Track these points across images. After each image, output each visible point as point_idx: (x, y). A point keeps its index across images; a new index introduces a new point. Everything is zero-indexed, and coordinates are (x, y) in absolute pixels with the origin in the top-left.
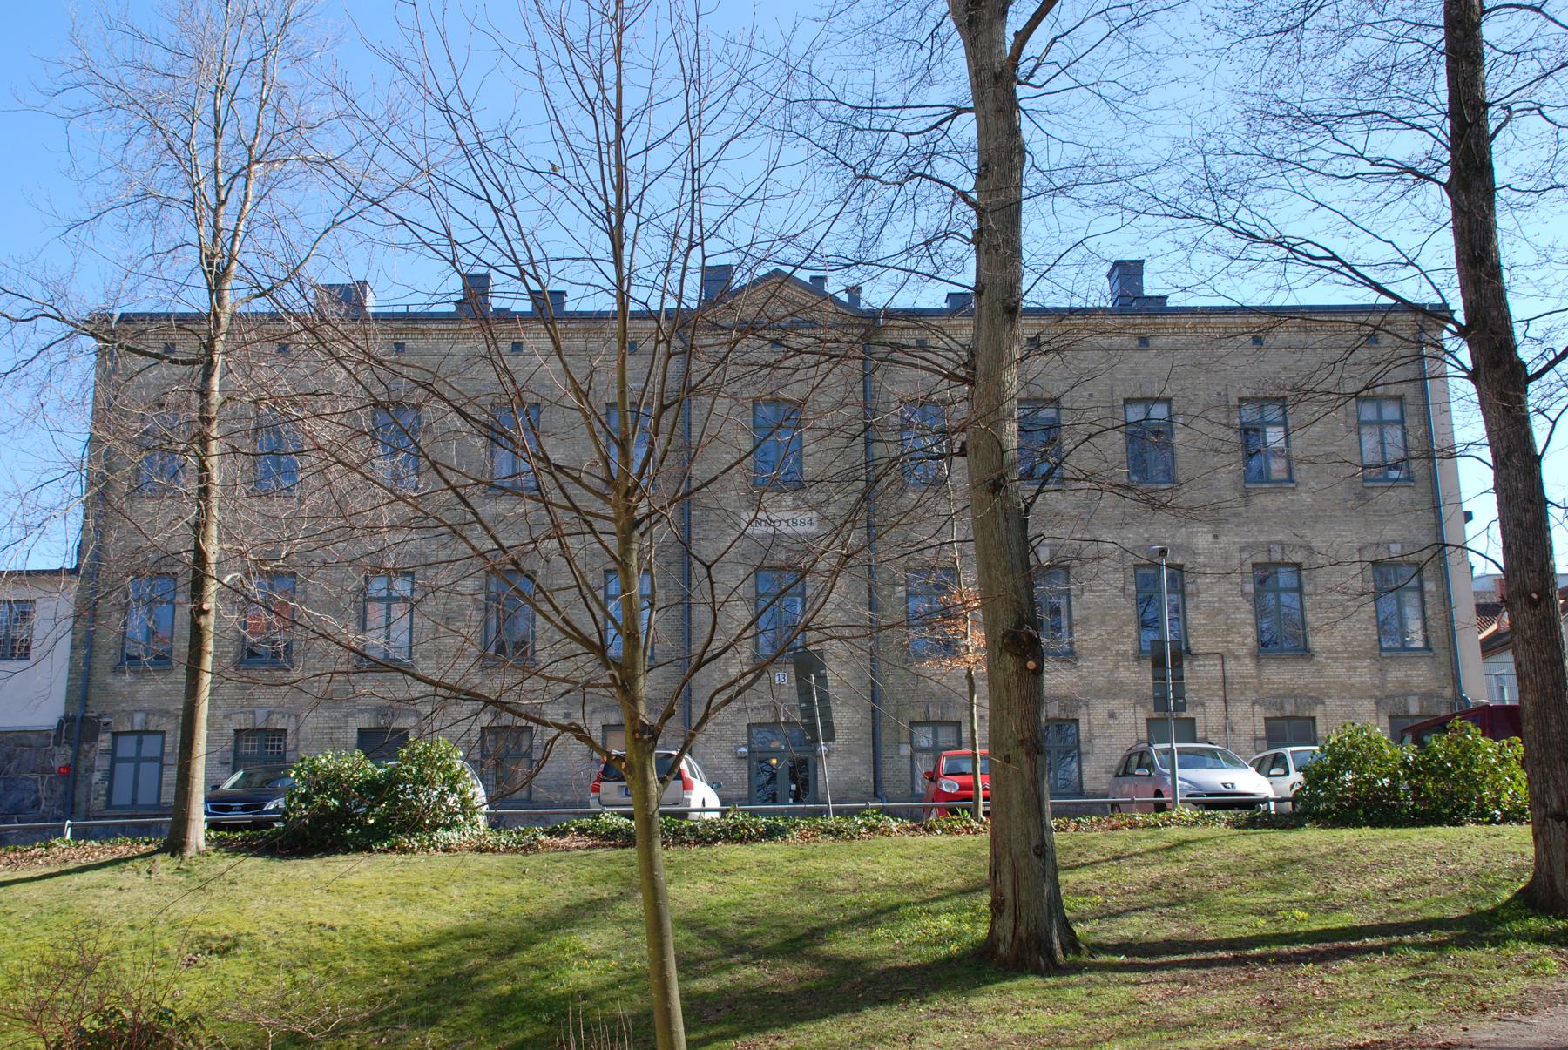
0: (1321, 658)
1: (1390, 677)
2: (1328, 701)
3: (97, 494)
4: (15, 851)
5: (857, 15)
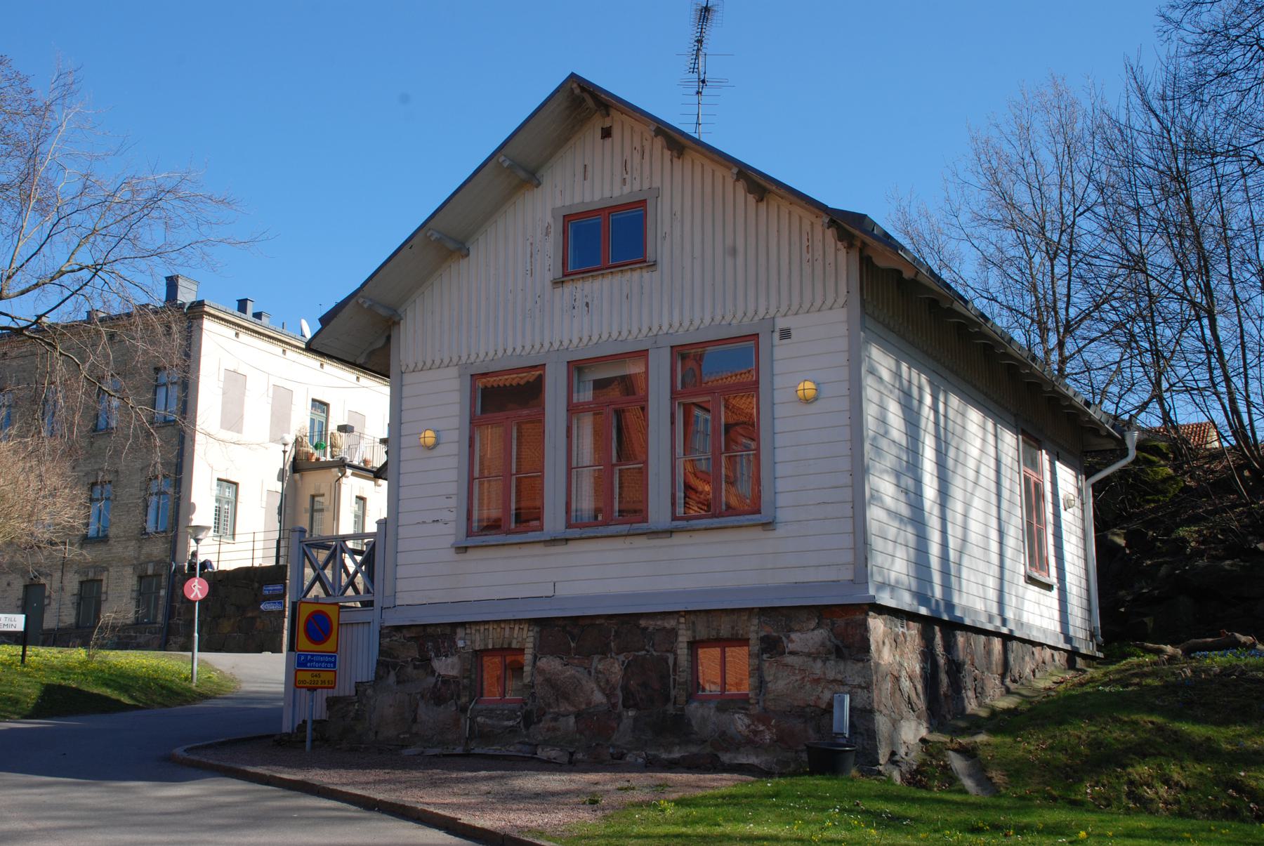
0: (111, 542)
1: (144, 551)
2: (111, 569)
3: (552, 708)
4: (870, 789)
5: (1262, 341)
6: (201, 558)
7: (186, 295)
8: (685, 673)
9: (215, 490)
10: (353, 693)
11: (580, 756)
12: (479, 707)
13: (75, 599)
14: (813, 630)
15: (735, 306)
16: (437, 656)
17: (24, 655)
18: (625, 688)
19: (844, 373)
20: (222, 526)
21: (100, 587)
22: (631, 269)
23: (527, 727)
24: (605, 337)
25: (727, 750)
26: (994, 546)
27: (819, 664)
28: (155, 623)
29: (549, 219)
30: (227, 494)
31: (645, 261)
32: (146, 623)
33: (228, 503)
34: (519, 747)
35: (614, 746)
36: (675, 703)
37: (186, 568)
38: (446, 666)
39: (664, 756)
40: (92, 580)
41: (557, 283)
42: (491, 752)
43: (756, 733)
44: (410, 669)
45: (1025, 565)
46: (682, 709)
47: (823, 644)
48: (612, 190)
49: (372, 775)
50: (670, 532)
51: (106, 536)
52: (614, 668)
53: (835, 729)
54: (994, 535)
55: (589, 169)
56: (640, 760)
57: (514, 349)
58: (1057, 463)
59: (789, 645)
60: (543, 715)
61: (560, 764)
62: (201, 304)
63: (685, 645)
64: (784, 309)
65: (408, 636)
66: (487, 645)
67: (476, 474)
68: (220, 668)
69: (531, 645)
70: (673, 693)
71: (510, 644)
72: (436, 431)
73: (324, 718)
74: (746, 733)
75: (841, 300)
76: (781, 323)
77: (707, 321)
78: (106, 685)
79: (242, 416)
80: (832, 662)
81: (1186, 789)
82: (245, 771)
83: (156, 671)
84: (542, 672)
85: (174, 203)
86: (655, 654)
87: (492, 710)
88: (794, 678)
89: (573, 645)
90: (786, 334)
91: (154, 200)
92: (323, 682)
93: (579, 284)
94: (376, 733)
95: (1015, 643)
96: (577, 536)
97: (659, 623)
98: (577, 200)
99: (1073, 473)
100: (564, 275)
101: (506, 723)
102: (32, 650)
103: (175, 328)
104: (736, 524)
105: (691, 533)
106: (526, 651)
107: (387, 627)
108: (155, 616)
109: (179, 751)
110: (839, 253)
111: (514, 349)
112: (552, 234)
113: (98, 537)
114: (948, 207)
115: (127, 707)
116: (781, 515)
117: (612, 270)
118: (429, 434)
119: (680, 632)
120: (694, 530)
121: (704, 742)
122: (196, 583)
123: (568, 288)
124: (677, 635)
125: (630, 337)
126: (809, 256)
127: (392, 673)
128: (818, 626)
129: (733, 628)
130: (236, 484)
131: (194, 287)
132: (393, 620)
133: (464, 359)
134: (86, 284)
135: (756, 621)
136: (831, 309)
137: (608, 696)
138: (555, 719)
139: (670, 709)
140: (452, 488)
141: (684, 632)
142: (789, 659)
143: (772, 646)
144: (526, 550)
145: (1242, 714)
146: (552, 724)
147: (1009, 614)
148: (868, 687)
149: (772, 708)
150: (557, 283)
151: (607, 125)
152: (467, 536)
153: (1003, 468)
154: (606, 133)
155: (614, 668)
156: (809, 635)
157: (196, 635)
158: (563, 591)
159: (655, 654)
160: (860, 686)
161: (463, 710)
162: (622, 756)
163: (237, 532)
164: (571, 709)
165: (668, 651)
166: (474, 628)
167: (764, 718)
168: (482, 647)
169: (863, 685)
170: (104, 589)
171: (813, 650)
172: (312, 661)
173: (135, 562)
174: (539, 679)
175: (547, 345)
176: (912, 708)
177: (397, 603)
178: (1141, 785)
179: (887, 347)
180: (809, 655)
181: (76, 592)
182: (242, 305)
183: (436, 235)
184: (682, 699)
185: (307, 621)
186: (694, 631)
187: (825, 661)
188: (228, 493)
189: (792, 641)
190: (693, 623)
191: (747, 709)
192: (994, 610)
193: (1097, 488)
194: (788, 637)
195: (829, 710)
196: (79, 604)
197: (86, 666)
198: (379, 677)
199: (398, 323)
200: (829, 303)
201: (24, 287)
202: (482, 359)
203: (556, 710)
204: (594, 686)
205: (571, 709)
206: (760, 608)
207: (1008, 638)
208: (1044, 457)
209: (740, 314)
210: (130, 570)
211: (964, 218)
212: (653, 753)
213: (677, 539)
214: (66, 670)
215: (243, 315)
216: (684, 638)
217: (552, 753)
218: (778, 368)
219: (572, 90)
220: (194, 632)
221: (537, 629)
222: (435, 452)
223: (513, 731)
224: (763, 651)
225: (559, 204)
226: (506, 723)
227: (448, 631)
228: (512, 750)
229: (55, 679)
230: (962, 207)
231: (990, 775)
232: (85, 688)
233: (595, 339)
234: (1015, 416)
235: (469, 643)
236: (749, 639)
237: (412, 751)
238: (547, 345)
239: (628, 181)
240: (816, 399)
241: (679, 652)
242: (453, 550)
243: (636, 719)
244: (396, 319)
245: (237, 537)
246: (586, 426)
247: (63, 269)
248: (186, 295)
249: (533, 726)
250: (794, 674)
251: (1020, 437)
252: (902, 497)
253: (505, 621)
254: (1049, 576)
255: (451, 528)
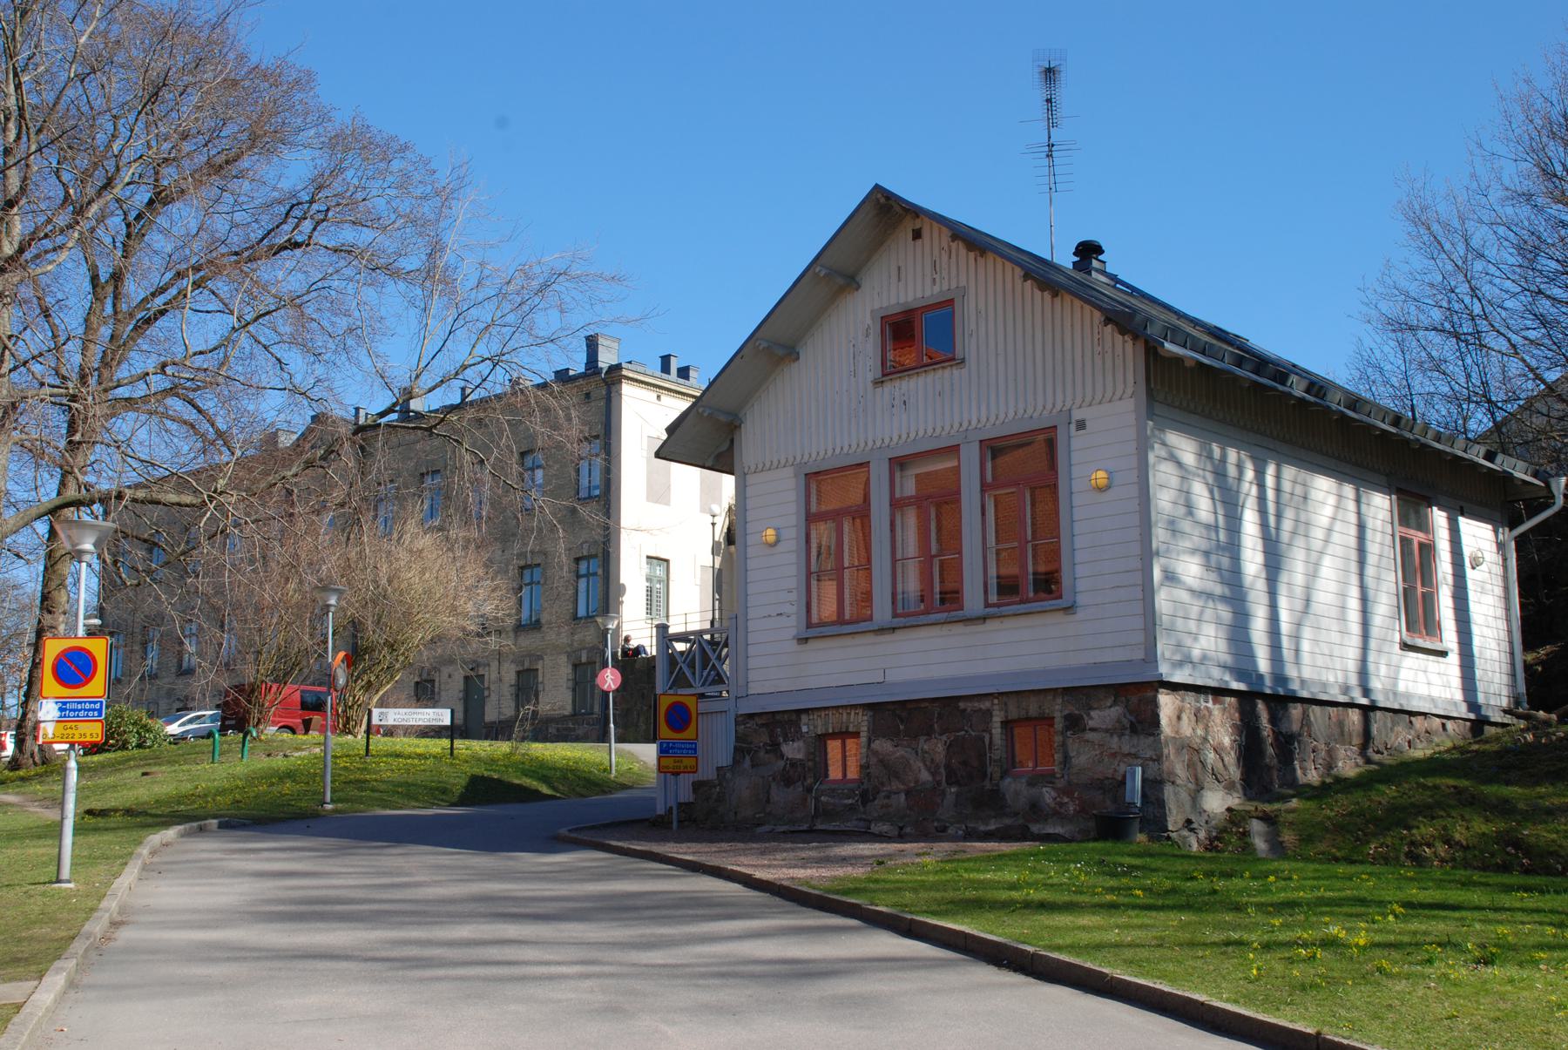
0: (544, 629)
6: (633, 644)
7: (606, 359)
8: (999, 752)
9: (645, 569)
10: (715, 777)
11: (908, 830)
12: (823, 787)
13: (513, 690)
14: (1111, 707)
15: (1035, 400)
16: (785, 741)
17: (452, 748)
18: (947, 766)
19: (1134, 462)
20: (654, 608)
21: (536, 677)
22: (934, 369)
23: (864, 803)
24: (921, 433)
25: (1037, 821)
26: (1354, 616)
27: (1116, 739)
28: (592, 714)
29: (869, 321)
30: (658, 572)
31: (954, 359)
32: (584, 714)
33: (659, 582)
34: (855, 823)
35: (938, 820)
36: (991, 779)
37: (619, 654)
38: (793, 750)
39: (982, 828)
40: (528, 670)
41: (878, 383)
42: (831, 828)
43: (1061, 804)
44: (762, 754)
45: (1400, 631)
46: (997, 785)
47: (1119, 721)
48: (924, 291)
49: (714, 847)
50: (984, 619)
51: (538, 621)
52: (937, 747)
53: (1128, 799)
54: (1354, 604)
55: (903, 268)
56: (960, 832)
57: (842, 449)
58: (1461, 519)
59: (1090, 722)
60: (878, 793)
61: (890, 837)
62: (618, 367)
63: (999, 725)
64: (1079, 401)
65: (759, 723)
66: (827, 729)
67: (814, 568)
68: (644, 759)
69: (866, 729)
70: (989, 770)
71: (847, 727)
72: (777, 529)
73: (691, 800)
74: (1053, 805)
75: (1129, 391)
76: (1077, 415)
77: (1011, 414)
78: (526, 773)
79: (669, 487)
80: (1127, 737)
81: (1466, 848)
82: (609, 845)
83: (577, 763)
84: (876, 753)
85: (567, 284)
86: (973, 734)
87: (834, 790)
88: (1094, 753)
89: (902, 727)
90: (1081, 425)
91: (545, 286)
92: (686, 767)
93: (897, 383)
94: (736, 813)
95: (1379, 713)
96: (901, 625)
97: (976, 704)
98: (893, 301)
99: (1490, 527)
100: (884, 375)
101: (846, 801)
102: (458, 743)
103: (574, 414)
104: (1039, 609)
105: (1002, 619)
106: (862, 734)
107: (742, 715)
108: (592, 707)
109: (563, 831)
110: (1126, 345)
111: (842, 449)
112: (871, 336)
113: (531, 624)
114: (1474, 185)
115: (559, 798)
116: (1081, 599)
117: (926, 369)
118: (770, 532)
119: (994, 713)
120: (1004, 616)
121: (1016, 814)
122: (608, 674)
123: (888, 387)
124: (991, 716)
125: (943, 433)
126: (1100, 349)
127: (748, 758)
128: (1115, 703)
129: (1040, 707)
130: (667, 561)
131: (615, 345)
132: (746, 708)
133: (798, 460)
134: (485, 380)
135: (1059, 701)
136: (1120, 399)
137: (933, 774)
138: (888, 797)
139: (988, 785)
140: (792, 583)
141: (998, 713)
142: (1090, 736)
143: (1074, 724)
144: (859, 640)
145: (1555, 776)
146: (886, 801)
147: (1376, 684)
148: (1158, 759)
149: (1075, 781)
150: (878, 383)
151: (918, 227)
152: (807, 628)
153: (1369, 534)
154: (917, 235)
155: (937, 747)
156: (1107, 712)
157: (612, 725)
158: (893, 676)
159: (973, 734)
160: (1151, 759)
161: (809, 790)
162: (944, 829)
163: (671, 613)
164: (902, 787)
165: (984, 731)
166: (816, 714)
167: (1067, 791)
168: (824, 732)
169: (1154, 757)
170: (540, 679)
171: (1110, 727)
172: (674, 748)
173: (569, 649)
174: (873, 760)
175: (870, 444)
176: (1217, 779)
177: (750, 692)
178: (1421, 845)
179: (1184, 428)
180: (1107, 731)
181: (513, 682)
182: (665, 362)
183: (765, 344)
184: (997, 775)
185: (666, 714)
186: (1006, 711)
187: (1121, 735)
188: (659, 571)
189: (1091, 718)
190: (1006, 704)
191: (1053, 783)
192: (1353, 680)
193: (1521, 542)
194: (1088, 715)
195: (1123, 783)
196: (517, 696)
197: (509, 758)
198: (736, 762)
199: (740, 426)
200: (1119, 393)
201: (430, 384)
202: (822, 457)
203: (889, 788)
204: (921, 765)
205: (902, 787)
206: (1064, 688)
207: (1368, 710)
208: (1439, 517)
209: (1040, 408)
210: (564, 658)
211: (1496, 194)
212: (972, 825)
213: (991, 625)
214: (491, 761)
215: (665, 376)
216: (997, 718)
217: (884, 828)
218: (1075, 457)
219: (878, 200)
220: (609, 723)
221: (870, 713)
222: (779, 548)
223: (852, 808)
224: (1067, 728)
225: (877, 306)
226: (846, 801)
227: (794, 717)
228: (850, 826)
229: (481, 771)
230: (1492, 183)
231: (1280, 839)
232: (505, 778)
233: (912, 435)
234: (1387, 475)
235: (812, 728)
236: (1054, 718)
237: (767, 828)
238: (870, 444)
239: (937, 280)
240: (1108, 487)
241: (993, 731)
242: (795, 641)
243: (958, 795)
244: (737, 424)
245: (670, 618)
246: (911, 519)
247: (466, 363)
248: (606, 359)
249: (869, 804)
250: (1094, 749)
251: (1394, 497)
252: (1213, 576)
253: (842, 706)
254: (1441, 641)
255: (793, 621)
